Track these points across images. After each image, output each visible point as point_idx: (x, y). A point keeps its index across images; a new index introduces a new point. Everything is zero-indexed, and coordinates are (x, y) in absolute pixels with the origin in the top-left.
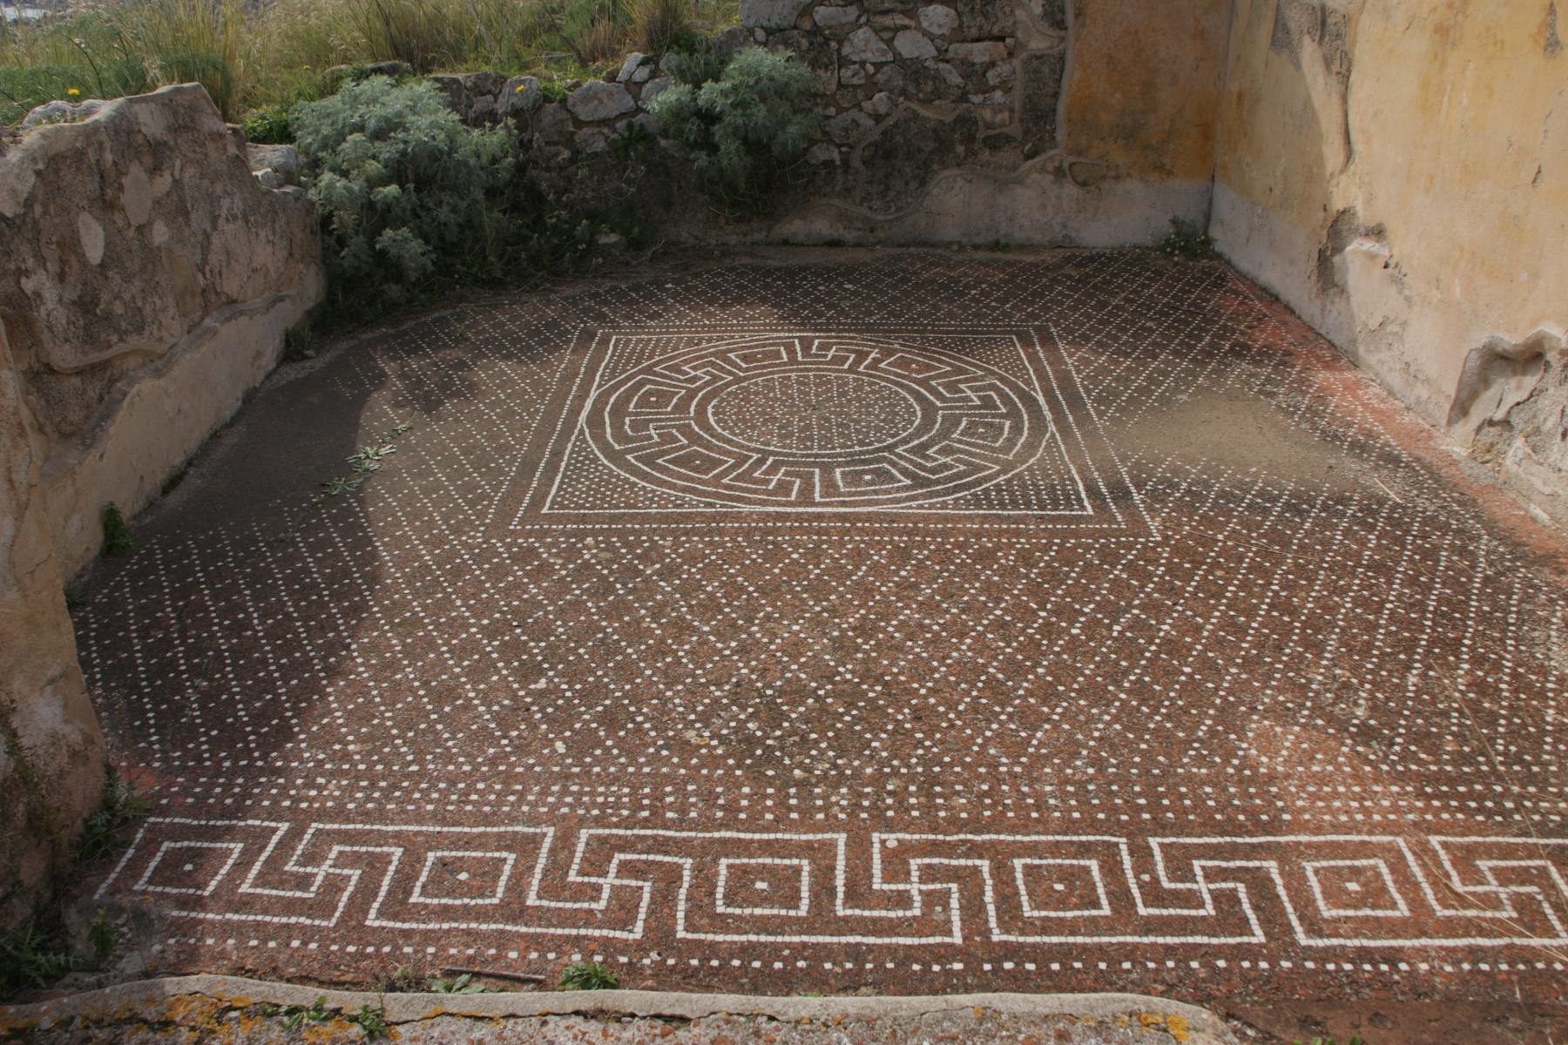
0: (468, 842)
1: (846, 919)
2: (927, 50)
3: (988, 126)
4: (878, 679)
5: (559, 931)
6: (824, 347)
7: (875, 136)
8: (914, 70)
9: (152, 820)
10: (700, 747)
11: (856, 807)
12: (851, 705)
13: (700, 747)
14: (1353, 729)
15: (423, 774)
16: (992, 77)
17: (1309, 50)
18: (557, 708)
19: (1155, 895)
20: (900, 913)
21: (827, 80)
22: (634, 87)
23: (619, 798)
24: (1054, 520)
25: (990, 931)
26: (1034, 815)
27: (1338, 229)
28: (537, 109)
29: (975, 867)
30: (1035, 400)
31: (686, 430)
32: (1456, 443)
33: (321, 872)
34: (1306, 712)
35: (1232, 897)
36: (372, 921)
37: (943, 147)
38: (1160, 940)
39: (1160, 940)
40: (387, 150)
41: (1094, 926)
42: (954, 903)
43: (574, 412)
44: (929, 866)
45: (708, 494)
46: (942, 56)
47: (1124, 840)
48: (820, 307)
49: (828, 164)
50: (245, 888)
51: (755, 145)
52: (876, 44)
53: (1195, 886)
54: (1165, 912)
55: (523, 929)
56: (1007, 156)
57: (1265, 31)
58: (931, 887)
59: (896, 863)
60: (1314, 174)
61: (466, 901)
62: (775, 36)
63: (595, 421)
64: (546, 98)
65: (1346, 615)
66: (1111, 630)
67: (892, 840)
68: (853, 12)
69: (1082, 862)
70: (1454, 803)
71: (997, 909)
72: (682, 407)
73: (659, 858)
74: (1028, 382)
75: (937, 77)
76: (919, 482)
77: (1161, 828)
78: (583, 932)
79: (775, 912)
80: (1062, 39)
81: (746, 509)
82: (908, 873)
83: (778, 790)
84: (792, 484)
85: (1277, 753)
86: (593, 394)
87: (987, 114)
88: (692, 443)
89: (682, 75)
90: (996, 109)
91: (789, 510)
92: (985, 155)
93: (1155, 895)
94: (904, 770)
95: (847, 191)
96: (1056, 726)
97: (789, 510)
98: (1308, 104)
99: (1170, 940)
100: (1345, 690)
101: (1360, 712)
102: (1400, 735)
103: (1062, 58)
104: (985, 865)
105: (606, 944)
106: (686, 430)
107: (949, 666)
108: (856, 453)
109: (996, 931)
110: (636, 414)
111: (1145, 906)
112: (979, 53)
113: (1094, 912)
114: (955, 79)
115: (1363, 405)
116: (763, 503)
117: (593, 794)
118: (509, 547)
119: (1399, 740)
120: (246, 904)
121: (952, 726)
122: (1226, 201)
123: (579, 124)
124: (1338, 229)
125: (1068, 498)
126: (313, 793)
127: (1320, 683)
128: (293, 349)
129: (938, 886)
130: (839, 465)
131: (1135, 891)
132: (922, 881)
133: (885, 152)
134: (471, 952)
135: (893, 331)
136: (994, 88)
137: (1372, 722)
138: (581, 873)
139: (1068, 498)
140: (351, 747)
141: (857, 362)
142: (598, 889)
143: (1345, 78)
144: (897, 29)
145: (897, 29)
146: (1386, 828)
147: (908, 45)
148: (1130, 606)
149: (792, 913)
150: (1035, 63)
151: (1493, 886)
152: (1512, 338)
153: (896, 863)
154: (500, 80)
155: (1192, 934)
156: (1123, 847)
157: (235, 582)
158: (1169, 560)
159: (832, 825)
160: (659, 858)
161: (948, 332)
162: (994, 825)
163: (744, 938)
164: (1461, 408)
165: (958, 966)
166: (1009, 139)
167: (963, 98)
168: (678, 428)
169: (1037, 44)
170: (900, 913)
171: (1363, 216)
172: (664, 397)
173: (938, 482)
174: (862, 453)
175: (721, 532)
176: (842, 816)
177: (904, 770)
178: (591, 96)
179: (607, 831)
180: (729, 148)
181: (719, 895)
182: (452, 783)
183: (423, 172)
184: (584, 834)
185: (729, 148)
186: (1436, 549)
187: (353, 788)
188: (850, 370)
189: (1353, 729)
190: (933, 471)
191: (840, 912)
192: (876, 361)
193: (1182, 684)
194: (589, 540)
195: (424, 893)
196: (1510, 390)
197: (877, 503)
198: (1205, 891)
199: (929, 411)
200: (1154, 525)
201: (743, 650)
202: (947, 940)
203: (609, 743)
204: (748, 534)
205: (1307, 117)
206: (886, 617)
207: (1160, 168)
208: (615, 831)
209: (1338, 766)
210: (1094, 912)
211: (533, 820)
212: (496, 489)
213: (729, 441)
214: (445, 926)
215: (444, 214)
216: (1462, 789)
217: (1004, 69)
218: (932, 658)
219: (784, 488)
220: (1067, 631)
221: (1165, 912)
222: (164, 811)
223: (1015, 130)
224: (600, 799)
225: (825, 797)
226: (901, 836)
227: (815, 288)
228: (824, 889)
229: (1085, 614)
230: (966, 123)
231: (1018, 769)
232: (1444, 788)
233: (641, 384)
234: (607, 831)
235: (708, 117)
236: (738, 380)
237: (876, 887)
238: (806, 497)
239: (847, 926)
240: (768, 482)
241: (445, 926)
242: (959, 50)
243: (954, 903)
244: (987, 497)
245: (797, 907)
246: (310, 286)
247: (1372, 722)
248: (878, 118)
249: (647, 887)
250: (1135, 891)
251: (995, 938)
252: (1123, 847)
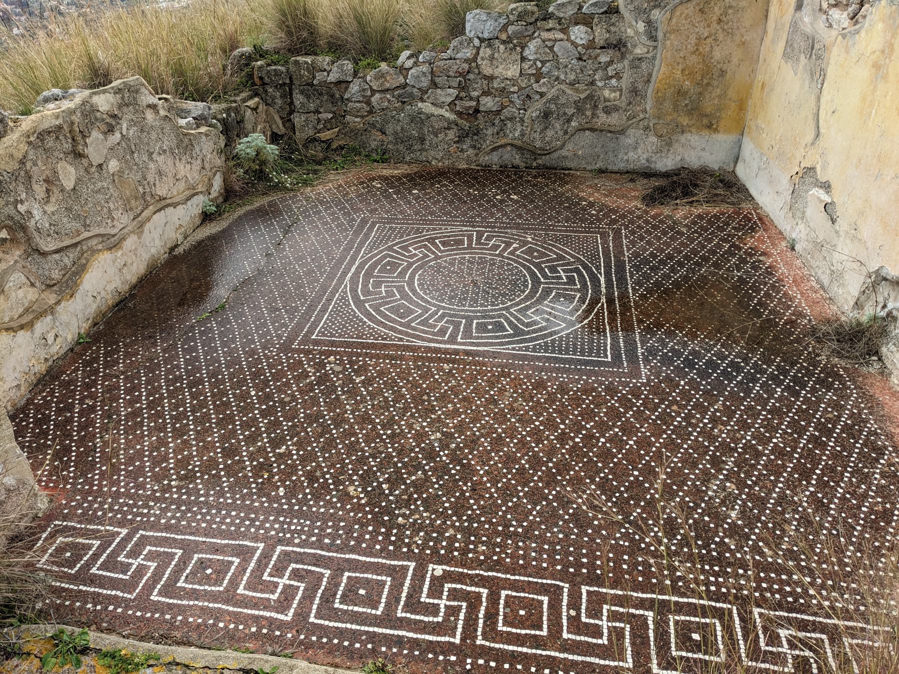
0: (216, 550)
1: (401, 619)
3: (606, 100)
4: (460, 463)
5: (249, 612)
6: (489, 238)
9: (57, 522)
10: (353, 498)
11: (425, 546)
12: (440, 478)
13: (353, 498)
14: (726, 526)
15: (206, 503)
18: (287, 465)
19: (576, 625)
20: (431, 619)
23: (303, 527)
24: (587, 363)
25: (476, 637)
26: (521, 562)
29: (479, 593)
30: (599, 281)
31: (401, 290)
33: (135, 563)
34: (700, 511)
35: (620, 633)
36: (154, 597)
38: (571, 657)
39: (571, 657)
41: (537, 642)
42: (462, 616)
43: (345, 274)
44: (455, 589)
45: (400, 332)
47: (567, 585)
48: (494, 210)
50: (94, 570)
53: (600, 623)
54: (578, 638)
55: (231, 609)
58: (452, 603)
59: (437, 585)
61: (206, 587)
63: (354, 281)
65: (745, 444)
66: (598, 441)
67: (439, 570)
69: (539, 598)
70: (776, 587)
71: (485, 622)
72: (402, 274)
73: (313, 568)
74: (598, 268)
76: (518, 332)
77: (593, 579)
78: (261, 613)
79: (365, 610)
80: (655, 47)
81: (420, 343)
82: (442, 593)
83: (387, 531)
84: (448, 328)
85: (674, 536)
86: (357, 263)
87: (606, 93)
88: (402, 298)
91: (442, 346)
93: (576, 625)
94: (457, 524)
96: (549, 503)
97: (442, 346)
99: (576, 658)
100: (729, 500)
101: (733, 514)
102: (755, 534)
104: (485, 592)
105: (271, 621)
106: (401, 290)
107: (500, 457)
108: (489, 311)
109: (480, 638)
110: (377, 277)
111: (568, 632)
113: (538, 633)
115: (802, 293)
116: (431, 341)
117: (290, 524)
118: (288, 358)
119: (753, 537)
120: (94, 581)
121: (492, 496)
122: (748, 147)
125: (598, 350)
126: (145, 511)
127: (714, 491)
129: (456, 603)
130: (477, 318)
131: (565, 622)
132: (448, 599)
134: (200, 621)
135: (529, 229)
136: (612, 77)
137: (740, 522)
138: (271, 575)
139: (598, 350)
140: (173, 483)
141: (504, 250)
142: (276, 585)
146: (719, 597)
148: (614, 425)
149: (374, 612)
150: (637, 62)
151: (785, 649)
153: (437, 585)
155: (590, 656)
156: (566, 590)
157: (139, 372)
158: (647, 397)
159: (409, 556)
160: (313, 568)
161: (561, 231)
162: (498, 565)
163: (344, 625)
165: (453, 658)
166: (616, 109)
168: (397, 287)
170: (431, 619)
172: (395, 266)
173: (528, 333)
174: (492, 310)
175: (402, 358)
176: (416, 551)
177: (457, 524)
179: (291, 549)
181: (338, 596)
182: (219, 511)
184: (279, 549)
186: (820, 400)
187: (167, 509)
188: (500, 255)
189: (726, 526)
190: (528, 325)
191: (400, 614)
192: (516, 249)
193: (631, 483)
194: (332, 358)
195: (186, 581)
197: (492, 344)
198: (605, 627)
199: (536, 282)
200: (644, 371)
201: (392, 436)
202: (452, 640)
203: (308, 491)
204: (416, 359)
206: (474, 420)
207: (709, 126)
208: (295, 549)
209: (709, 551)
210: (538, 633)
211: (255, 539)
212: (291, 320)
213: (422, 299)
214: (191, 603)
216: (784, 577)
218: (492, 450)
219: (443, 331)
220: (573, 439)
221: (578, 638)
222: (65, 518)
224: (293, 527)
225: (411, 538)
226: (444, 567)
227: (494, 196)
228: (394, 598)
229: (586, 429)
231: (520, 530)
232: (773, 575)
233: (385, 257)
234: (291, 549)
236: (437, 257)
237: (422, 600)
238: (453, 340)
239: (402, 623)
240: (435, 326)
241: (191, 603)
243: (462, 616)
244: (553, 346)
245: (377, 609)
247: (740, 522)
249: (302, 586)
250: (565, 622)
251: (478, 642)
252: (566, 590)
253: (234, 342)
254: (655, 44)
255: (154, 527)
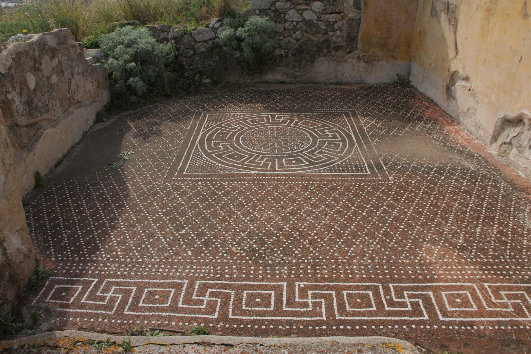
0: (159, 285)
1: (286, 311)
2: (314, 17)
3: (335, 43)
4: (297, 230)
5: (189, 315)
6: (279, 118)
7: (296, 46)
8: (309, 24)
10: (237, 253)
11: (290, 273)
12: (288, 239)
13: (237, 253)
14: (458, 247)
15: (143, 262)
16: (336, 26)
17: (443, 17)
18: (189, 240)
19: (391, 303)
20: (305, 309)
21: (280, 27)
22: (215, 29)
23: (210, 270)
24: (357, 176)
25: (335, 315)
26: (350, 276)
27: (453, 78)
28: (182, 37)
29: (330, 294)
30: (351, 136)
31: (232, 146)
32: (493, 150)
33: (109, 295)
34: (442, 241)
35: (417, 304)
36: (126, 312)
37: (319, 50)
38: (393, 318)
39: (393, 318)
40: (131, 51)
41: (370, 314)
42: (323, 306)
43: (194, 140)
44: (315, 293)
45: (240, 167)
46: (319, 19)
47: (381, 285)
48: (278, 104)
49: (280, 56)
50: (83, 301)
51: (256, 49)
52: (297, 15)
53: (405, 300)
54: (394, 309)
55: (177, 315)
56: (341, 53)
57: (428, 10)
58: (315, 300)
59: (303, 292)
60: (445, 59)
61: (158, 305)
62: (262, 12)
63: (201, 143)
64: (185, 33)
65: (456, 208)
66: (376, 213)
67: (302, 284)
68: (289, 4)
69: (366, 292)
70: (492, 272)
71: (338, 308)
72: (231, 138)
73: (223, 291)
74: (348, 130)
75: (317, 26)
76: (311, 163)
77: (393, 280)
78: (197, 316)
79: (262, 309)
80: (360, 13)
81: (253, 172)
82: (308, 296)
83: (264, 268)
84: (268, 164)
85: (433, 255)
86: (201, 134)
87: (334, 39)
88: (234, 150)
89: (231, 25)
90: (337, 37)
91: (267, 173)
92: (334, 53)
93: (391, 303)
94: (306, 261)
95: (287, 65)
96: (358, 246)
97: (267, 173)
98: (443, 35)
99: (396, 318)
100: (455, 234)
101: (460, 241)
102: (474, 249)
103: (360, 20)
104: (333, 293)
105: (205, 320)
106: (232, 146)
107: (321, 226)
108: (290, 154)
109: (337, 315)
110: (216, 140)
111: (388, 307)
112: (332, 18)
113: (371, 309)
114: (323, 27)
115: (462, 137)
116: (259, 170)
117: (201, 269)
118: (172, 185)
119: (474, 251)
120: (83, 306)
121: (322, 246)
122: (415, 68)
123: (196, 42)
124: (453, 78)
125: (362, 169)
126: (106, 269)
127: (447, 231)
128: (99, 118)
129: (318, 300)
130: (284, 157)
131: (385, 302)
132: (312, 298)
133: (300, 51)
134: (159, 322)
135: (302, 112)
136: (337, 30)
137: (465, 245)
138: (197, 296)
139: (362, 169)
140: (119, 253)
141: (290, 123)
142: (202, 301)
143: (455, 26)
144: (304, 10)
145: (304, 10)
147: (307, 15)
148: (383, 205)
149: (268, 309)
150: (351, 21)
151: (506, 300)
152: (512, 115)
153: (303, 292)
154: (169, 27)
155: (404, 316)
156: (380, 287)
157: (80, 197)
158: (396, 190)
159: (282, 279)
160: (223, 291)
161: (321, 113)
162: (337, 279)
163: (252, 318)
164: (495, 138)
165: (324, 327)
166: (342, 47)
167: (326, 33)
168: (230, 145)
169: (351, 15)
170: (305, 309)
171: (462, 73)
172: (225, 135)
173: (318, 163)
174: (292, 153)
175: (244, 180)
176: (285, 276)
177: (306, 261)
178: (200, 33)
179: (206, 282)
180: (247, 50)
181: (244, 303)
182: (153, 265)
183: (143, 58)
184: (198, 282)
185: (247, 50)
186: (486, 186)
187: (119, 267)
188: (288, 125)
189: (458, 247)
190: (316, 160)
191: (285, 309)
192: (297, 122)
193: (400, 232)
194: (200, 183)
195: (143, 302)
196: (511, 132)
197: (297, 170)
198: (408, 302)
199: (315, 139)
200: (391, 178)
201: (252, 220)
202: (321, 318)
203: (206, 252)
204: (253, 181)
205: (443, 40)
206: (300, 209)
207: (393, 57)
208: (208, 282)
209: (453, 260)
210: (371, 309)
211: (181, 278)
212: (168, 166)
213: (247, 150)
214: (151, 314)
215: (150, 72)
216: (495, 267)
217: (340, 23)
218: (316, 223)
219: (265, 165)
220: (361, 214)
221: (394, 309)
222: (56, 275)
223: (344, 44)
224: (203, 271)
225: (279, 270)
226: (305, 283)
227: (276, 97)
228: (279, 301)
229: (367, 208)
230: (327, 42)
231: (345, 261)
232: (489, 267)
233: (217, 130)
234: (206, 282)
235: (240, 40)
236: (250, 129)
237: (297, 300)
238: (273, 168)
239: (287, 314)
240: (260, 163)
241: (151, 314)
242: (325, 17)
243: (323, 306)
244: (334, 168)
245: (270, 307)
246: (105, 97)
247: (465, 245)
248: (297, 40)
249: (219, 300)
250: (385, 302)
251: (337, 318)
252: (380, 287)
253: (135, 178)
254: (360, 11)
255: (115, 276)
